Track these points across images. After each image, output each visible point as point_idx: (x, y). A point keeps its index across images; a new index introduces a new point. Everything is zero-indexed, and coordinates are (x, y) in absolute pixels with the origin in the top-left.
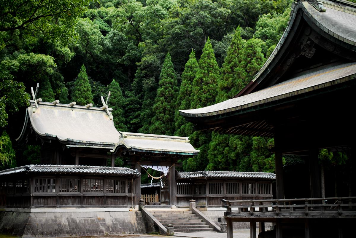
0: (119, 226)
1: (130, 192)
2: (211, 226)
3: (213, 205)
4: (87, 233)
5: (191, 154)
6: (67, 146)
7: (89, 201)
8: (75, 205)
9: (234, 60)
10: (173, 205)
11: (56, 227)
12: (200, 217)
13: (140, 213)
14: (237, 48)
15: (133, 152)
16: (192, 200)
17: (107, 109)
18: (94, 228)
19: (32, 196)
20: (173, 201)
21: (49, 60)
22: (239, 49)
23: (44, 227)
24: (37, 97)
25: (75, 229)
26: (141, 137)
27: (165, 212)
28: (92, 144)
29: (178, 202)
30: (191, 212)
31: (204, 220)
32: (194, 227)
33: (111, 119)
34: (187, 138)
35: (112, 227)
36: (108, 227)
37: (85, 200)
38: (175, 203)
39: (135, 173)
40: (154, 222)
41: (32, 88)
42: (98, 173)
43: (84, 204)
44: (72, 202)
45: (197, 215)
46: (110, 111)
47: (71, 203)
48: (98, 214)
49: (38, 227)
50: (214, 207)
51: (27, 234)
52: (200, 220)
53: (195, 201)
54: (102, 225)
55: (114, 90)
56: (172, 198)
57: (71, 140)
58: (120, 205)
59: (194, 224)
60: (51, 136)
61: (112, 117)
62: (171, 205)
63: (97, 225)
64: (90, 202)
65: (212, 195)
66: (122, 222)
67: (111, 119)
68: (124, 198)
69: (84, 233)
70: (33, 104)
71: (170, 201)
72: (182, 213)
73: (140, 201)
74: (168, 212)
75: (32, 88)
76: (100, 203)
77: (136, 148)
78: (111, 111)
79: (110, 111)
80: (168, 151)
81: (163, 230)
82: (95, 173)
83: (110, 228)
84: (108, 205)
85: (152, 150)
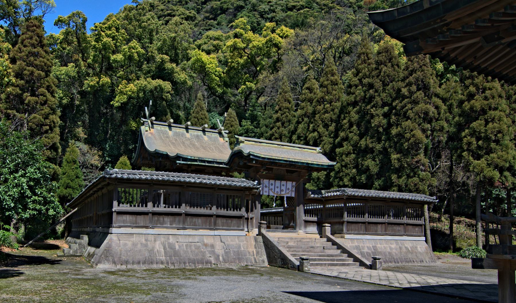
0: (232, 255)
1: (247, 211)
2: (356, 259)
3: (352, 231)
4: (189, 263)
5: (325, 167)
6: (178, 162)
7: (194, 221)
8: (174, 226)
9: (363, 71)
10: (300, 229)
11: (147, 254)
12: (339, 247)
13: (260, 238)
14: (366, 58)
15: (253, 159)
16: (327, 225)
17: (223, 132)
18: (200, 257)
19: (115, 212)
20: (300, 226)
21: (167, 85)
22: (368, 59)
23: (129, 254)
24: (150, 116)
25: (173, 258)
26: (262, 144)
27: (291, 239)
28: (204, 161)
29: (305, 227)
30: (325, 239)
31: (344, 251)
32: (333, 260)
33: (227, 142)
34: (318, 149)
35: (223, 256)
36: (218, 256)
37: (188, 219)
38: (303, 227)
39: (254, 185)
40: (281, 253)
41: (146, 108)
42: (206, 184)
43: (186, 224)
44: (170, 221)
45: (334, 243)
46: (225, 133)
47: (169, 223)
48: (205, 238)
49: (121, 254)
50: (354, 234)
51: (104, 263)
52: (339, 251)
53: (329, 225)
54: (209, 253)
55: (231, 119)
56: (298, 221)
57: (181, 156)
58: (234, 226)
59: (332, 256)
60: (161, 152)
61: (227, 139)
62: (297, 229)
63: (203, 254)
64: (195, 222)
65: (351, 219)
66: (236, 250)
67: (227, 142)
68: (240, 217)
69: (185, 263)
70: (146, 123)
71: (296, 225)
72: (314, 240)
73: (261, 223)
74: (296, 238)
75: (146, 108)
76: (208, 224)
77: (256, 154)
78: (227, 133)
79: (225, 133)
80: (296, 160)
81: (293, 263)
82: (201, 183)
83: (221, 258)
84: (219, 226)
85: (276, 158)
